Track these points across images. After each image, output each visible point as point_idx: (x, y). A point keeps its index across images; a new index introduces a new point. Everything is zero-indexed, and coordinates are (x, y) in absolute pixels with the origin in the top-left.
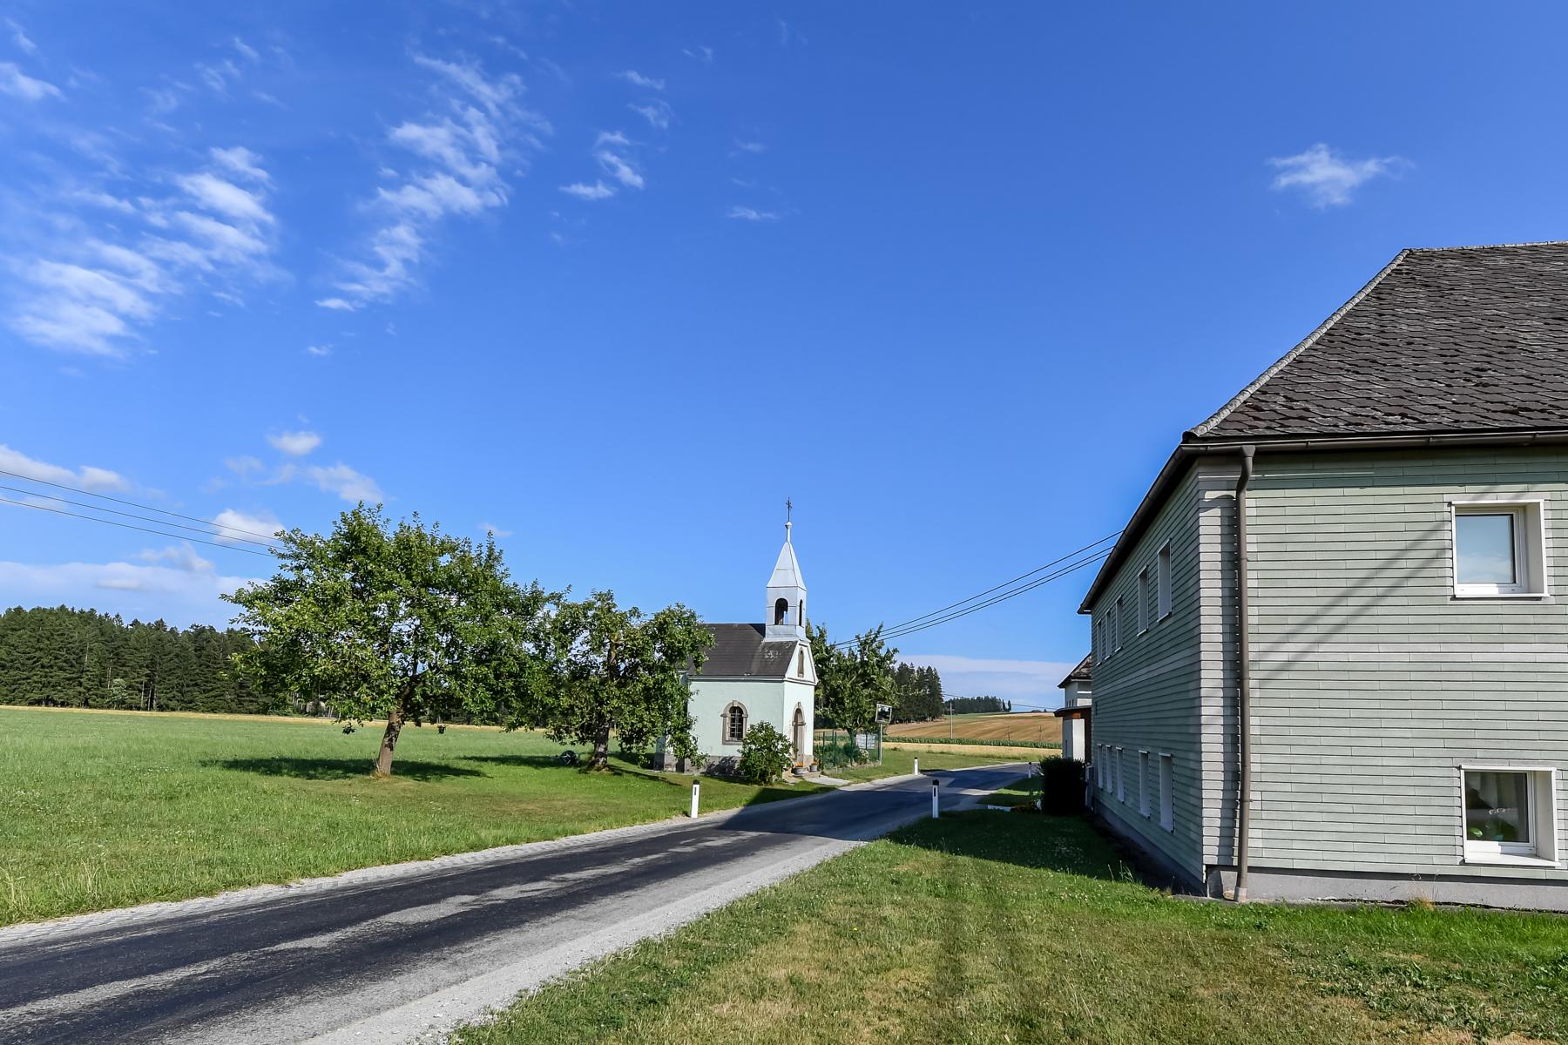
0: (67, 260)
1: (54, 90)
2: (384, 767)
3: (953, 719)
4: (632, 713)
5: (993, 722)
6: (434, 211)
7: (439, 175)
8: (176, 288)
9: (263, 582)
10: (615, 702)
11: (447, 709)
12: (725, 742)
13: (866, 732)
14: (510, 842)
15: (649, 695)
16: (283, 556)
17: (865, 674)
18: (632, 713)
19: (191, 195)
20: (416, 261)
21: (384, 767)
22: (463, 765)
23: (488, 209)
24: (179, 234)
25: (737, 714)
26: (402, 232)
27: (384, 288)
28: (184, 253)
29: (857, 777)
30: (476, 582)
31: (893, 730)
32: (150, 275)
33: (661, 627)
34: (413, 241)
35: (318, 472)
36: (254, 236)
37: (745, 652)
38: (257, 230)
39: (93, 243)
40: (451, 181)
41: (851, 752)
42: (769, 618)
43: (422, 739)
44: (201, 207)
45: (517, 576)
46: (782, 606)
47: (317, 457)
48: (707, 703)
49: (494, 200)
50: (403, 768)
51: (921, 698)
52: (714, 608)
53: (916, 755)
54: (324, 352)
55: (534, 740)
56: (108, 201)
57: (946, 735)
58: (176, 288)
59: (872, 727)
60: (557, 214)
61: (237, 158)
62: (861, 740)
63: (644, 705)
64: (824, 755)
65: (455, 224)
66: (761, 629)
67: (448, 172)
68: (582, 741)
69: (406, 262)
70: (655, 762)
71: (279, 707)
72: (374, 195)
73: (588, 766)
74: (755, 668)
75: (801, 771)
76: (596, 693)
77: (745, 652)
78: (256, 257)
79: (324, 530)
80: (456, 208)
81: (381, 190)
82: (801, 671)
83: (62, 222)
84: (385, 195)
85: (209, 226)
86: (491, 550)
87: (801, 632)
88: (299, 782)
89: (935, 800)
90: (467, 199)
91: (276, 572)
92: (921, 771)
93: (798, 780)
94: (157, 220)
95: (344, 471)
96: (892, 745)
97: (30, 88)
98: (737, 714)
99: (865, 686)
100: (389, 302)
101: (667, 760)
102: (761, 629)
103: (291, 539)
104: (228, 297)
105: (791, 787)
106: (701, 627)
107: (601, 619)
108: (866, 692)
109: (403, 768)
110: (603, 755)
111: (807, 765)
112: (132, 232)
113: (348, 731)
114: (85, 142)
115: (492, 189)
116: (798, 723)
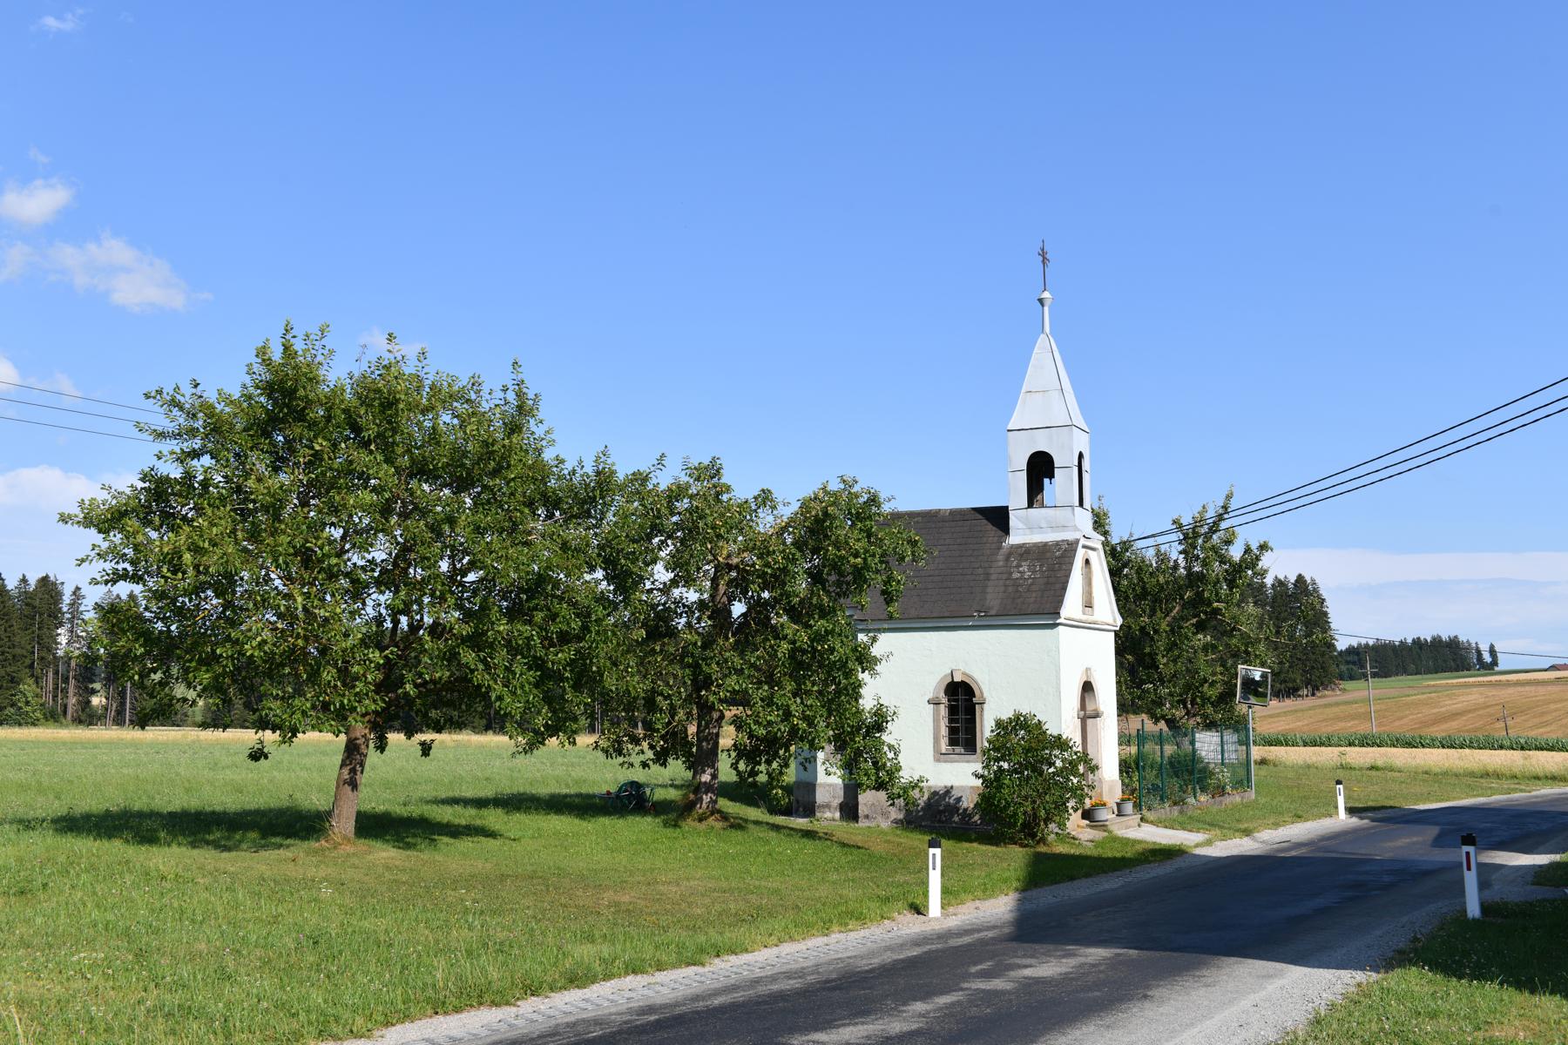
2: (344, 824)
4: (769, 702)
5: (1455, 694)
9: (127, 482)
10: (732, 682)
11: (459, 704)
12: (940, 756)
13: (1210, 725)
14: (634, 969)
15: (800, 664)
16: (161, 435)
17: (1199, 601)
18: (769, 702)
21: (344, 824)
22: (446, 814)
25: (960, 700)
30: (489, 464)
33: (816, 525)
35: (68, 255)
37: (978, 568)
42: (1014, 493)
43: (405, 767)
45: (570, 443)
46: (1040, 468)
47: (70, 227)
48: (904, 673)
50: (373, 826)
51: (1299, 644)
52: (913, 486)
53: (1342, 774)
54: (68, 26)
55: (580, 761)
57: (1363, 728)
62: (1207, 744)
63: (790, 686)
64: (1160, 778)
66: (998, 517)
68: (661, 758)
70: (802, 801)
73: (675, 813)
74: (993, 599)
75: (1104, 815)
76: (696, 667)
77: (978, 568)
79: (228, 378)
82: (1088, 605)
86: (520, 395)
87: (1084, 520)
88: (206, 857)
89: (1471, 879)
91: (147, 462)
92: (1351, 811)
93: (1097, 835)
95: (117, 250)
98: (960, 700)
99: (1201, 627)
101: (821, 797)
102: (998, 517)
103: (175, 403)
105: (1090, 850)
106: (897, 516)
107: (695, 517)
108: (1203, 639)
109: (373, 826)
110: (709, 788)
113: (257, 755)
116: (1088, 715)
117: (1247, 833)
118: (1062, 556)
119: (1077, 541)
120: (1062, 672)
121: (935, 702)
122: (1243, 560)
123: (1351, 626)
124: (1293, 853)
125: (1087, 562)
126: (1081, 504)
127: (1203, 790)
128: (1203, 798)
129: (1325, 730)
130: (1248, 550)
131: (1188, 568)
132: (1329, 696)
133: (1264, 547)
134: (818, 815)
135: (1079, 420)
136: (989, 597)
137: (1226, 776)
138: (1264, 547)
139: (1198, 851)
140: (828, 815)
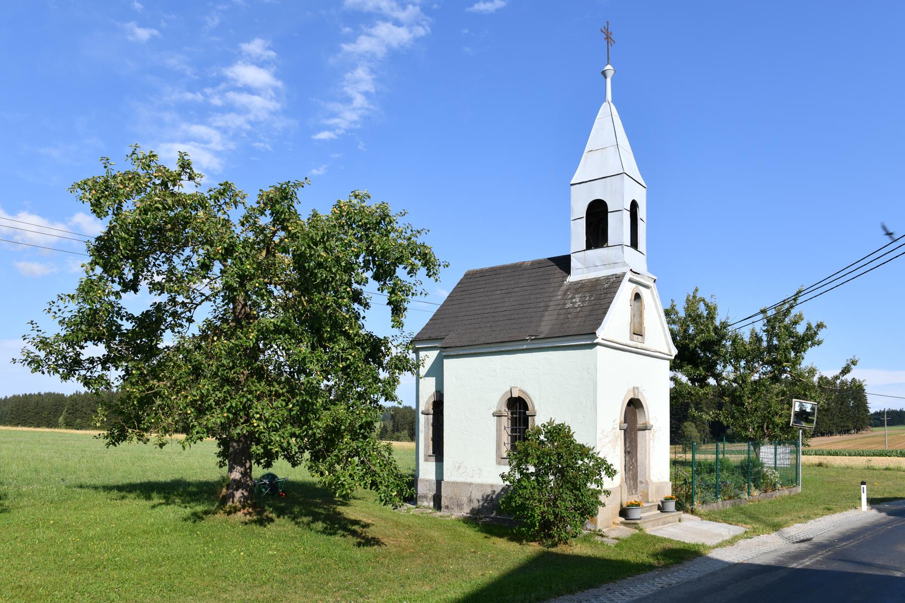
0: (172, 141)
1: (155, 32)
3: (878, 431)
6: (381, 52)
7: (380, 22)
8: (232, 146)
19: (233, 79)
20: (373, 91)
23: (417, 40)
24: (229, 108)
26: (361, 73)
27: (354, 116)
28: (234, 121)
29: (764, 543)
31: (817, 442)
32: (216, 138)
34: (368, 78)
36: (271, 98)
38: (272, 93)
39: (184, 126)
40: (389, 25)
41: (750, 472)
44: (239, 85)
46: (597, 215)
49: (421, 31)
56: (189, 96)
57: (880, 448)
58: (232, 146)
59: (784, 435)
60: (466, 31)
61: (256, 47)
65: (396, 57)
67: (385, 19)
69: (366, 94)
71: (56, 425)
72: (340, 50)
77: (533, 305)
78: (273, 113)
80: (395, 44)
81: (343, 46)
82: (638, 332)
83: (167, 117)
84: (347, 47)
85: (243, 99)
90: (402, 35)
92: (872, 502)
94: (216, 101)
96: (815, 459)
97: (143, 34)
100: (359, 126)
102: (564, 263)
104: (262, 145)
111: (656, 499)
112: (202, 113)
114: (174, 61)
115: (418, 24)
117: (776, 527)
118: (609, 287)
119: (624, 274)
120: (610, 389)
121: (498, 415)
122: (805, 335)
123: (875, 405)
124: (807, 563)
125: (637, 296)
126: (634, 244)
127: (757, 487)
128: (756, 493)
129: (861, 448)
130: (809, 328)
131: (769, 341)
132: (864, 434)
133: (820, 326)
134: (419, 503)
135: (632, 167)
136: (543, 323)
137: (775, 476)
138: (820, 326)
139: (716, 554)
140: (425, 504)
